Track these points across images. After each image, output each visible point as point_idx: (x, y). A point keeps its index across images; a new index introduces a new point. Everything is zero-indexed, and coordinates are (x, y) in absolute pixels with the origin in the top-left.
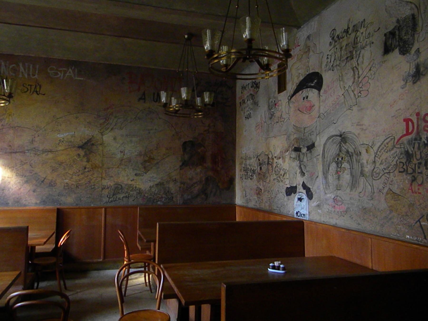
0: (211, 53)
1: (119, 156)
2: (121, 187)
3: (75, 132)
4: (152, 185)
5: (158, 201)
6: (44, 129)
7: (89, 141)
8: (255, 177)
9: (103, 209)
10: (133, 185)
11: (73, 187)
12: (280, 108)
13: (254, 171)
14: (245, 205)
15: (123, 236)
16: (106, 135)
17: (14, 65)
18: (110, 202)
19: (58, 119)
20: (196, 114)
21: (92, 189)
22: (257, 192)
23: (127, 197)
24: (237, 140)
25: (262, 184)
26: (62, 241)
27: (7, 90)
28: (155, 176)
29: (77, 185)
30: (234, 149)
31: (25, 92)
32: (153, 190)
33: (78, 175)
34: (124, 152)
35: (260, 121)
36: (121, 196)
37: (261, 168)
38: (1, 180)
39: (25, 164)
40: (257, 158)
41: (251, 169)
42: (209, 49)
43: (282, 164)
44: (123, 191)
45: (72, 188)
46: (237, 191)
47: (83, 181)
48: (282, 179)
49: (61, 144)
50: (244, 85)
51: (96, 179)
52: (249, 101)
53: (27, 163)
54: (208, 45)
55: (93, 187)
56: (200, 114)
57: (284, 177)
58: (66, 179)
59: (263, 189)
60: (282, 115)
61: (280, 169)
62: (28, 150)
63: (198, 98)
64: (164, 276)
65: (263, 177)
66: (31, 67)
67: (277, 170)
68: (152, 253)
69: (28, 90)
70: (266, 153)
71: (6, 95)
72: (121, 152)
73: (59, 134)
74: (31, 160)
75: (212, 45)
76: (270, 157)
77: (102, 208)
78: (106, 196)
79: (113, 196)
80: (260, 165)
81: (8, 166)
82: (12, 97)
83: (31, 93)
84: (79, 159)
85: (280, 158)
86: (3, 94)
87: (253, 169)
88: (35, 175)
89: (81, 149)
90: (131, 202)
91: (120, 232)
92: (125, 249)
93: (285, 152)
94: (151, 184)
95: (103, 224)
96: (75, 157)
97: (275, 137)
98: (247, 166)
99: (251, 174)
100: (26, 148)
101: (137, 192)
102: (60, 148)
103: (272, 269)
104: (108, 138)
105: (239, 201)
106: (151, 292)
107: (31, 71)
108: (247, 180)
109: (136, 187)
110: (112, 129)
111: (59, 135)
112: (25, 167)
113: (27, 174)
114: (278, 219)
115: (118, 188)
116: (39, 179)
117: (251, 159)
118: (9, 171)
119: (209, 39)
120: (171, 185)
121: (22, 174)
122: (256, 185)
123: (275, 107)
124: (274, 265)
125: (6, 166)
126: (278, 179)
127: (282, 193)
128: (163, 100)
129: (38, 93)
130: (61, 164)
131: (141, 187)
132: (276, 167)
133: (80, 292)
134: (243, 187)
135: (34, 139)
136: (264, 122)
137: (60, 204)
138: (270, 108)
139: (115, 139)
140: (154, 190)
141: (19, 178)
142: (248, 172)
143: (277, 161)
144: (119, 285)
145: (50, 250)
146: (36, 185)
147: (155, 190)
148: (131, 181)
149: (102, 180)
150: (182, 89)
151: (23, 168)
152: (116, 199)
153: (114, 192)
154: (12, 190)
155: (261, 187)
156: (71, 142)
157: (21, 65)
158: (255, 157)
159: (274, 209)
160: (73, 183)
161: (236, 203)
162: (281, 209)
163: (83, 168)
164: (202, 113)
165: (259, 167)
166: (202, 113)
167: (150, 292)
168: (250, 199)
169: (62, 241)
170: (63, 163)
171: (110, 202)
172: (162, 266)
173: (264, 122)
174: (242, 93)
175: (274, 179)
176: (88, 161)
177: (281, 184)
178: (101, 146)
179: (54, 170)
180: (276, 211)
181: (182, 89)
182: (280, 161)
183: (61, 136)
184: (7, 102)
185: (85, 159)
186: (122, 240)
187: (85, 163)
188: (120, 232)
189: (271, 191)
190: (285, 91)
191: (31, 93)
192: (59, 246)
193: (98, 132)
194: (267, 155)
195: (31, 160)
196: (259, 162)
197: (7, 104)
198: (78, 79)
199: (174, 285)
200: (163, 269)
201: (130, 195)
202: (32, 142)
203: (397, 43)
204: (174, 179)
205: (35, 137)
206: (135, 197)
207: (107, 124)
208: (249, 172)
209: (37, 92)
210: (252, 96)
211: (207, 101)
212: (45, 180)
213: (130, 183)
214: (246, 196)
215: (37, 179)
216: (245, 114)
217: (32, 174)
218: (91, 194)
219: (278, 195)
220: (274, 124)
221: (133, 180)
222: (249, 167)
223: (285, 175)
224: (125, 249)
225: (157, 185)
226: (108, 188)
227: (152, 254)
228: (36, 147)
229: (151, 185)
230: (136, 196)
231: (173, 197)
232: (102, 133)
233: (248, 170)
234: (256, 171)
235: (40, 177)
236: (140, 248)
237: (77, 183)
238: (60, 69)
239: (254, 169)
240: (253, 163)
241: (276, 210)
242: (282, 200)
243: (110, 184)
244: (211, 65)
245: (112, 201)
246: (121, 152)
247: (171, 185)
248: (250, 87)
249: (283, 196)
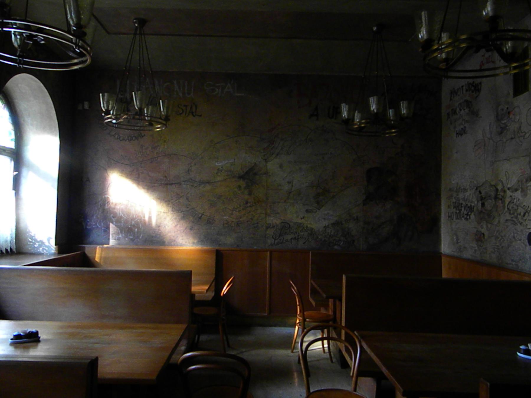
0: (428, 43)
1: (286, 188)
2: (288, 225)
3: (235, 159)
4: (327, 224)
5: (335, 245)
6: (200, 157)
7: (251, 169)
8: (472, 216)
9: (268, 252)
10: (304, 224)
11: (233, 225)
12: (518, 118)
13: (471, 209)
14: (456, 254)
15: (295, 288)
16: (270, 162)
17: (168, 84)
18: (276, 244)
19: (215, 144)
20: (387, 131)
21: (254, 227)
22: (477, 237)
23: (296, 239)
24: (443, 166)
25: (485, 226)
26: (225, 290)
27: (164, 113)
28: (332, 213)
29: (238, 223)
30: (439, 178)
31: (181, 114)
32: (328, 230)
33: (239, 211)
34: (293, 183)
35: (482, 138)
36: (289, 237)
37: (483, 205)
38: (157, 216)
39: (181, 197)
40: (477, 189)
41: (467, 205)
42: (425, 37)
43: (521, 199)
44: (292, 231)
45: (232, 227)
46: (442, 235)
47: (245, 218)
48: (520, 220)
49: (219, 174)
50: (454, 89)
51: (260, 216)
52: (462, 110)
53: (183, 196)
54: (424, 33)
55: (255, 225)
56: (393, 131)
57: (525, 218)
58: (225, 216)
59: (486, 233)
60: (520, 127)
61: (517, 206)
62: (184, 181)
63: (390, 110)
64: (361, 347)
65: (486, 217)
66: (186, 84)
67: (513, 207)
68: (330, 311)
69: (183, 112)
70: (493, 183)
71: (163, 118)
72: (289, 182)
73: (217, 162)
74: (187, 194)
75: (430, 32)
76: (500, 187)
77: (267, 251)
78: (271, 237)
79: (279, 237)
80: (481, 200)
81: (164, 200)
82: (169, 120)
83: (187, 114)
84: (239, 192)
85: (516, 190)
86: (159, 117)
87: (469, 205)
88: (193, 210)
89: (242, 180)
90: (301, 245)
91: (291, 282)
92: (298, 304)
93: (527, 181)
94: (326, 223)
95: (268, 271)
96: (236, 190)
97: (508, 160)
98: (459, 201)
99: (465, 212)
100: (182, 179)
101: (308, 233)
102: (219, 179)
103: (524, 354)
104: (272, 165)
105: (445, 248)
106: (332, 362)
107: (186, 89)
108: (459, 221)
109: (307, 227)
110: (277, 155)
111: (218, 163)
112: (181, 200)
113: (184, 209)
114: (515, 277)
115: (285, 227)
116: (196, 214)
117: (467, 191)
118: (164, 205)
119: (426, 24)
120: (352, 225)
121: (178, 209)
122: (475, 228)
123: (509, 117)
124: (527, 348)
125: (161, 200)
126: (513, 221)
127: (520, 240)
128: (345, 114)
129: (194, 114)
130: (220, 197)
131: (313, 227)
132: (510, 202)
133: (245, 351)
134: (452, 230)
135: (190, 168)
136: (489, 139)
137: (220, 245)
138: (499, 119)
139: (281, 166)
140: (329, 231)
141: (175, 213)
142: (461, 210)
143: (511, 194)
144: (304, 352)
145: (210, 298)
146: (193, 222)
147: (331, 231)
148: (301, 219)
149: (266, 217)
150: (371, 99)
151: (179, 202)
152: (283, 241)
153: (281, 232)
154: (168, 227)
155: (483, 231)
156: (230, 171)
157: (175, 82)
158: (473, 189)
159: (507, 264)
160: (234, 220)
161: (442, 252)
162: (520, 264)
163: (245, 202)
164: (396, 130)
165: (480, 202)
166: (396, 130)
167: (330, 361)
168: (465, 248)
169: (225, 290)
170: (221, 196)
171: (276, 244)
172: (355, 332)
173: (489, 139)
174: (451, 100)
175: (507, 220)
176: (250, 194)
177: (519, 227)
178: (264, 175)
179: (212, 205)
180: (511, 266)
181: (371, 99)
182: (518, 194)
183: (218, 164)
184: (165, 126)
185: (246, 192)
186: (294, 292)
187: (246, 197)
188: (291, 282)
189: (502, 237)
190: (527, 92)
191: (187, 114)
192: (222, 294)
193: (262, 158)
194: (494, 186)
195: (187, 194)
196: (480, 195)
197: (164, 128)
198: (239, 94)
199: (380, 363)
200: (359, 337)
201: (300, 237)
202: (189, 171)
203: (133, 136)
204: (355, 218)
205: (191, 166)
206: (305, 239)
207: (272, 149)
208: (463, 209)
209: (192, 113)
210: (468, 104)
211: (404, 114)
212: (203, 216)
213: (300, 221)
214: (458, 243)
215: (194, 215)
216: (457, 129)
217: (189, 209)
218: (254, 234)
219: (514, 244)
220: (506, 141)
221: (304, 218)
222: (464, 203)
223: (527, 214)
224: (298, 304)
225: (333, 224)
226: (273, 227)
227: (331, 313)
228: (193, 178)
229: (325, 224)
230: (307, 238)
231: (354, 241)
232: (265, 160)
233: (462, 207)
234: (475, 208)
235: (197, 213)
236: (314, 303)
237: (238, 220)
238: (217, 85)
239: (471, 205)
240: (470, 196)
241: (510, 264)
242: (520, 250)
243: (276, 223)
244: (429, 60)
245: (278, 244)
246: (289, 182)
247: (352, 225)
248: (464, 92)
249: (524, 246)
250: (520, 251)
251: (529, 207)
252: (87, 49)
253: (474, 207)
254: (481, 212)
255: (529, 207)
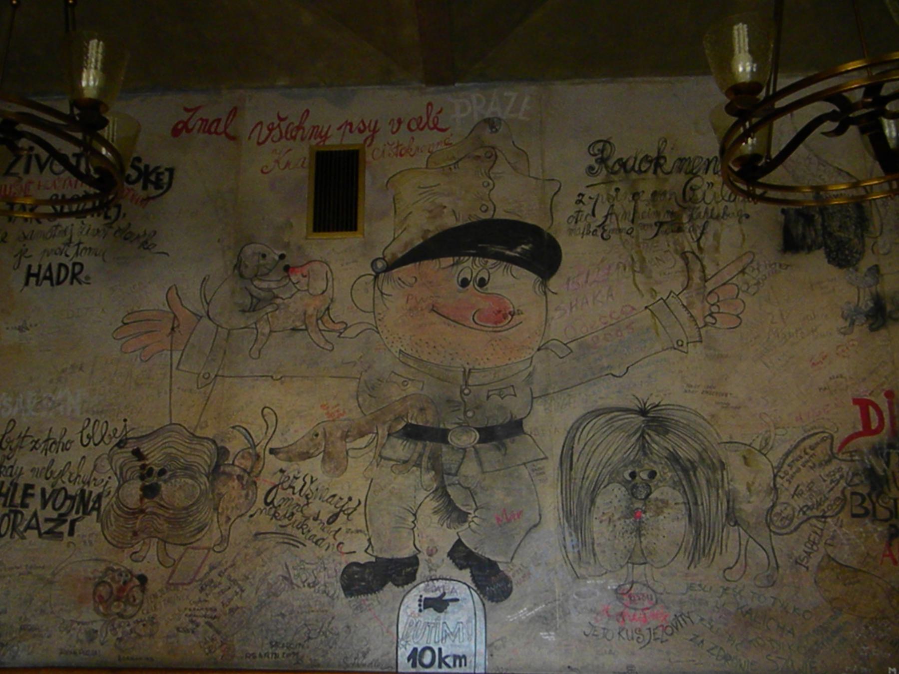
57: (334, 527)
177: (309, 552)
182: (314, 467)
223: (342, 517)
250: (312, 615)
251: (350, 499)
252: (107, 150)
253: (99, 497)
254: (135, 513)
255: (350, 499)
